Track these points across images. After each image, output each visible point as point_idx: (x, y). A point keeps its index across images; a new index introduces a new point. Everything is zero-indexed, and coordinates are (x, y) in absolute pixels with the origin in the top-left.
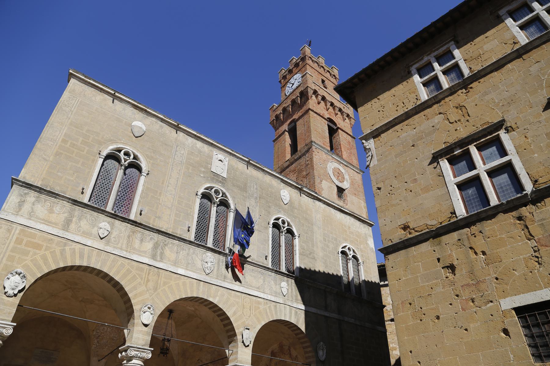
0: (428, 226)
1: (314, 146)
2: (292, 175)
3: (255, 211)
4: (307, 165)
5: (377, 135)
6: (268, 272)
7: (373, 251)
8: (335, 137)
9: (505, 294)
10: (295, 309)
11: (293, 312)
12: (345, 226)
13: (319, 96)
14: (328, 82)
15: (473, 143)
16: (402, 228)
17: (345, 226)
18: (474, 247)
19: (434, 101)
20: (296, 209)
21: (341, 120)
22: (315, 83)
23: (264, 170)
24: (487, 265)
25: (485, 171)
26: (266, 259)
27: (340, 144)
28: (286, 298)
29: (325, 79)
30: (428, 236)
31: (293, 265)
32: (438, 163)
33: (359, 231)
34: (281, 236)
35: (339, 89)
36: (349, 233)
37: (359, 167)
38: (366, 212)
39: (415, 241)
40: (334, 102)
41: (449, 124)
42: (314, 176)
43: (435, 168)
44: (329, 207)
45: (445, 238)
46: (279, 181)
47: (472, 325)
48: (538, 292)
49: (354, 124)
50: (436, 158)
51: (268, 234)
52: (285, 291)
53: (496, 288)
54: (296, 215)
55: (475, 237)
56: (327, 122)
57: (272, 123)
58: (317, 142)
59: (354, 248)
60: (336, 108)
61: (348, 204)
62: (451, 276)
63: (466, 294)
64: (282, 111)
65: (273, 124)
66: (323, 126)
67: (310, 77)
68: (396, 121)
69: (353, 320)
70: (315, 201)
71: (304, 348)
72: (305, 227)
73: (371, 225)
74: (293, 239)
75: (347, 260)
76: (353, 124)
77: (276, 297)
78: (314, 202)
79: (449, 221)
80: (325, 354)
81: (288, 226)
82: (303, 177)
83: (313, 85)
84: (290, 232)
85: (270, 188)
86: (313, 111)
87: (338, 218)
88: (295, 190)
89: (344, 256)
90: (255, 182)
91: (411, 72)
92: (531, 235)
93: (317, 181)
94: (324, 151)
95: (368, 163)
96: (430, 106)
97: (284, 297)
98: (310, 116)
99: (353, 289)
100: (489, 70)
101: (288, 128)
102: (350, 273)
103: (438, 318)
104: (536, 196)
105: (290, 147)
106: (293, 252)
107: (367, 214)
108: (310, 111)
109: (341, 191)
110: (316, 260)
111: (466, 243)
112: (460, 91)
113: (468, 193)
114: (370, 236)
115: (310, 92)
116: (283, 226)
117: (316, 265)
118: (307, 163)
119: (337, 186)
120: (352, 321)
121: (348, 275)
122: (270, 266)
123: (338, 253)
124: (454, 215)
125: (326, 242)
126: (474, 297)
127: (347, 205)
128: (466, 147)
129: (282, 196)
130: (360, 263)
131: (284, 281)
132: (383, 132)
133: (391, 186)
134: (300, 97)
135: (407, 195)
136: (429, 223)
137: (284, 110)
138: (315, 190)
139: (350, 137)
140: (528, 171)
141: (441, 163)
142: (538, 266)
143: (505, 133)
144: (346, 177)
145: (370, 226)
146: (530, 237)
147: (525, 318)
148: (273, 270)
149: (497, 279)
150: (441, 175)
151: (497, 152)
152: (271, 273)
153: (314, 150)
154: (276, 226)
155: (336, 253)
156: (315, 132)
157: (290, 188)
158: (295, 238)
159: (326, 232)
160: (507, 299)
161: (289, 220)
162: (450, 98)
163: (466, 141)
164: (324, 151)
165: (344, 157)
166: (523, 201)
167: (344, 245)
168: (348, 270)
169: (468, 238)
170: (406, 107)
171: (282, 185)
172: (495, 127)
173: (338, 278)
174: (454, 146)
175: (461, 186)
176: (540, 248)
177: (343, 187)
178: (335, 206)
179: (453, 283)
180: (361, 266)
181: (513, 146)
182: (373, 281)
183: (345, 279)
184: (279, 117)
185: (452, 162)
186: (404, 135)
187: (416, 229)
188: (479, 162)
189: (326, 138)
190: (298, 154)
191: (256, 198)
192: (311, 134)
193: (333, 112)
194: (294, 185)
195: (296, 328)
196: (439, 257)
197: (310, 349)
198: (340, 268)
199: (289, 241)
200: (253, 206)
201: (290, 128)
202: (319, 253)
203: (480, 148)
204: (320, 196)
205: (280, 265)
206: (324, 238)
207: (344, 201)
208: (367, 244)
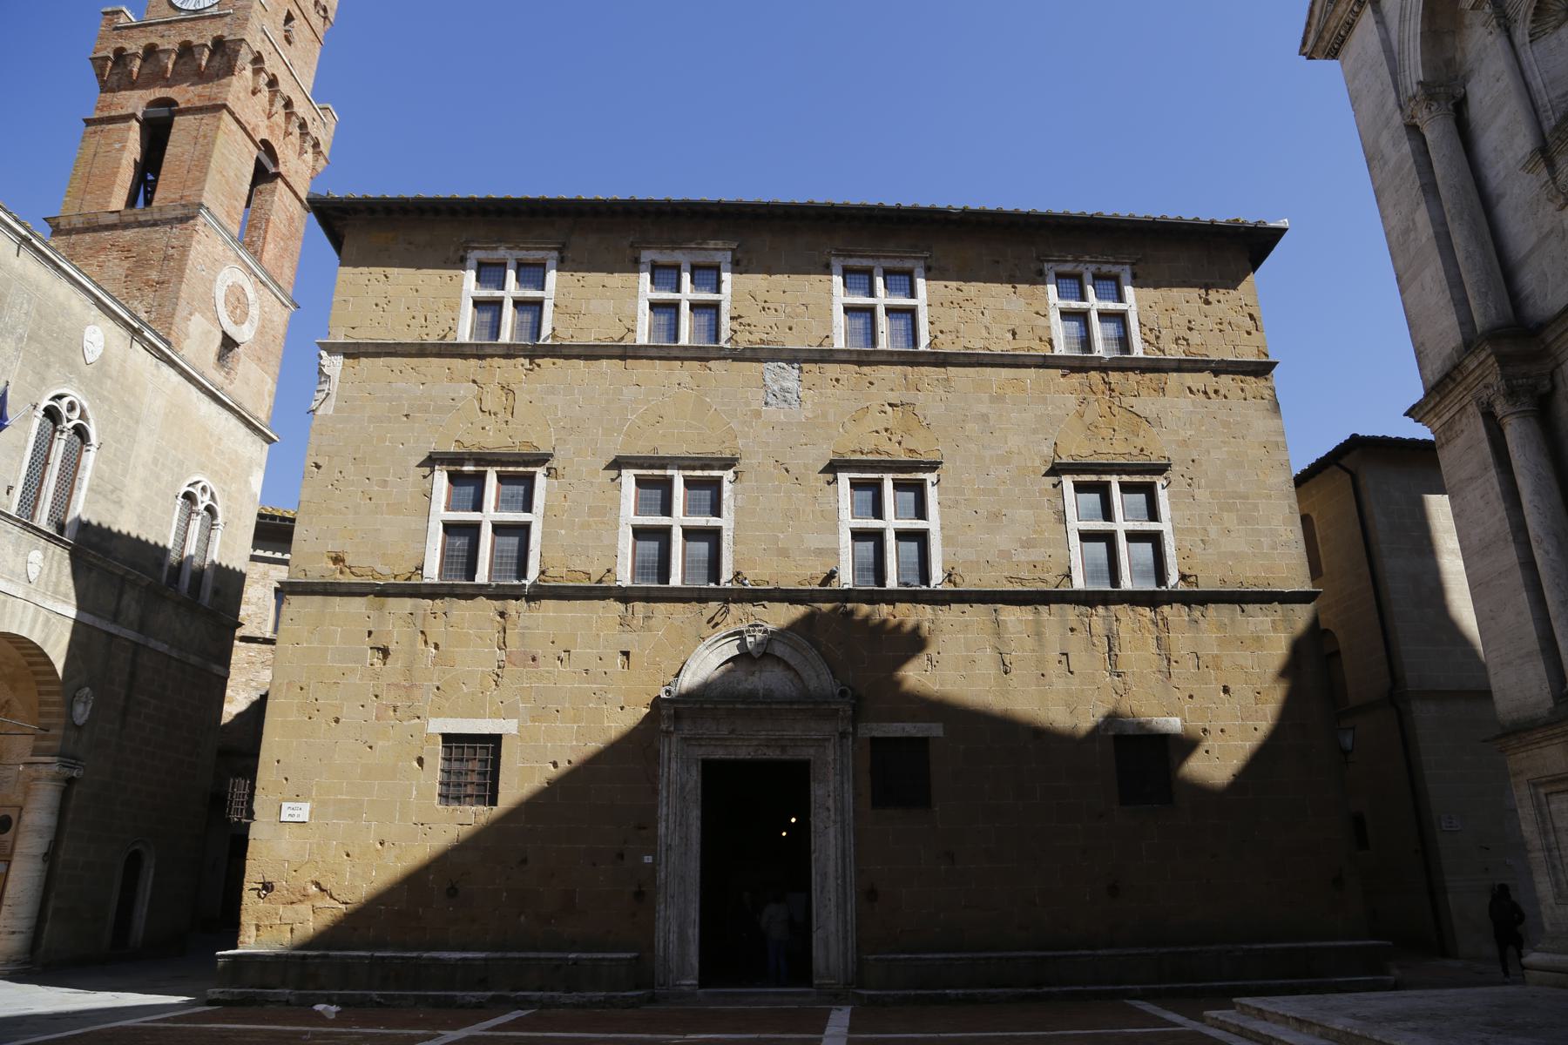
0: (374, 573)
1: (204, 217)
2: (114, 259)
3: (9, 371)
4: (167, 258)
5: (353, 354)
6: (5, 523)
7: (256, 499)
8: (261, 193)
9: (439, 712)
10: (46, 612)
11: (41, 619)
12: (211, 435)
13: (264, 74)
14: (301, 24)
15: (497, 466)
16: (332, 558)
18: (427, 633)
19: (475, 352)
20: (111, 378)
21: (295, 152)
22: (265, 34)
23: (58, 268)
24: (434, 665)
25: (491, 522)
26: (8, 493)
27: (268, 221)
28: (32, 586)
29: (296, 12)
30: (368, 589)
31: (66, 513)
32: (432, 472)
34: (56, 441)
35: (318, 205)
37: (290, 292)
38: (270, 406)
39: (344, 589)
40: (293, 101)
41: (479, 411)
42: (177, 299)
43: (425, 477)
44: (190, 385)
45: (393, 603)
46: (90, 302)
47: (380, 743)
48: (478, 721)
49: (323, 172)
50: (432, 461)
51: (27, 433)
52: (34, 572)
53: (432, 701)
54: (106, 393)
55: (435, 618)
56: (255, 152)
57: (99, 63)
58: (212, 210)
59: (214, 490)
60: (294, 118)
61: (236, 382)
62: (378, 664)
63: (388, 698)
64: (144, 52)
65: (102, 68)
66: (242, 163)
67: (260, 12)
68: (399, 349)
69: (167, 646)
70: (161, 363)
71: (40, 693)
72: (119, 425)
73: (270, 441)
74: (81, 449)
75: (190, 514)
76: (320, 170)
77: (10, 583)
78: (157, 365)
79: (409, 578)
80: (88, 713)
81: (80, 418)
82: (146, 283)
83: (258, 39)
84: (81, 432)
85: (63, 316)
86: (232, 114)
88: (121, 331)
89: (188, 503)
90: (28, 295)
91: (466, 259)
92: (504, 643)
93: (182, 310)
94: (221, 235)
95: (314, 405)
96: (465, 357)
97: (29, 585)
98: (218, 127)
99: (185, 579)
100: (575, 352)
101: (144, 113)
102: (188, 542)
103: (337, 721)
104: (534, 591)
105: (133, 170)
106: (73, 481)
107: (271, 411)
108: (225, 111)
109: (229, 344)
110: (122, 507)
111: (419, 623)
112: (522, 360)
113: (454, 544)
114: (260, 466)
115: (245, 58)
116: (67, 418)
117: (119, 518)
118: (171, 251)
119: (224, 333)
120: (164, 648)
121: (183, 548)
122: (13, 511)
123: (177, 497)
124: (420, 572)
125: (156, 466)
126: (399, 704)
127: (232, 382)
128: (483, 466)
129: (85, 342)
130: (218, 525)
131: (37, 549)
132: (367, 355)
133: (341, 472)
134: (210, 50)
135: (362, 502)
136: (379, 568)
137: (151, 51)
138: (169, 334)
139: (299, 204)
140: (543, 551)
141: (436, 473)
142: (494, 687)
143: (545, 475)
144: (254, 311)
145: (267, 442)
146: (502, 645)
147: (451, 748)
148: (18, 521)
149: (438, 688)
150: (428, 495)
151: (521, 498)
152: (12, 526)
153: (200, 228)
154: (52, 414)
155: (172, 495)
156: (218, 177)
157: (110, 323)
158: (89, 450)
159: (164, 443)
160: (439, 720)
161: (86, 405)
162: (503, 362)
163: (489, 458)
164: (221, 235)
165: (266, 256)
166: (517, 592)
167: (196, 479)
168: (186, 537)
169: (425, 615)
170: (426, 331)
171: (92, 313)
172: (536, 458)
173: (164, 551)
174: (467, 457)
175: (450, 528)
176: (507, 664)
177: (236, 339)
178: (203, 386)
179: (377, 676)
180: (219, 532)
181: (544, 502)
182: (231, 567)
183: (174, 557)
184: (128, 60)
185: (454, 478)
186: (402, 385)
187: (353, 570)
188: (489, 503)
189: (239, 199)
190: (152, 213)
191: (21, 339)
192: (205, 180)
193: (283, 125)
194: (122, 318)
195: (36, 652)
196: (372, 629)
197: (56, 698)
198: (170, 532)
199: (71, 453)
200: (9, 356)
201: (151, 116)
202: (134, 491)
203: (501, 478)
204: (176, 353)
205: (35, 508)
206: (155, 458)
207: (228, 373)
208: (247, 482)
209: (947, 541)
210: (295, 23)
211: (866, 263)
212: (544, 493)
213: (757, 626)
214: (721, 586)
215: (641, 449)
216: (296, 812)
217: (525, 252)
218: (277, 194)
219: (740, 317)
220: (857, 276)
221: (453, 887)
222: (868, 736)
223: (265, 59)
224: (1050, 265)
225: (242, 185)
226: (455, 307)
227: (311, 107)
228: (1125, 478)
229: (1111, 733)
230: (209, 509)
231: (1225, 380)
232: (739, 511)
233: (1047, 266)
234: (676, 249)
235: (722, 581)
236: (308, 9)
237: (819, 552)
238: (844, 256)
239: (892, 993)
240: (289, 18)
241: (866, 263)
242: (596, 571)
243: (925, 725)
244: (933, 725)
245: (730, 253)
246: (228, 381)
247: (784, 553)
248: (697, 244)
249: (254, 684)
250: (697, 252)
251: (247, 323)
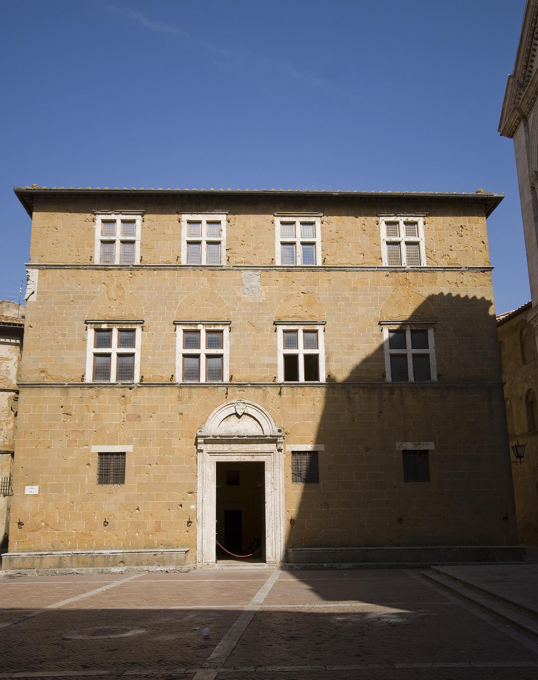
9: (96, 443)
47: (70, 457)
215: (185, 317)
216: (33, 490)
224: (383, 218)
226: (92, 245)
232: (232, 348)
237: (268, 365)
247: (252, 366)
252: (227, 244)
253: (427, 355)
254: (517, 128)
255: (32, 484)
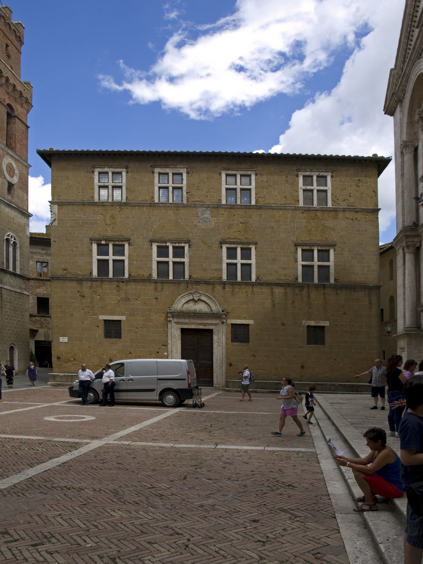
14: (12, 47)
17: (11, 218)
27: (15, 135)
33: (21, 221)
36: (13, 224)
47: (86, 322)
87: (7, 211)
91: (94, 172)
136: (79, 272)
144: (17, 172)
150: (91, 250)
160: (102, 316)
167: (8, 233)
185: (99, 245)
198: (4, 252)
207: (12, 196)
209: (257, 267)
210: (9, 48)
211: (234, 172)
212: (128, 251)
213: (196, 291)
214: (185, 280)
216: (64, 340)
217: (114, 169)
218: (16, 124)
219: (189, 192)
220: (231, 177)
221: (111, 359)
222: (231, 323)
223: (3, 71)
225: (4, 124)
227: (23, 85)
228: (320, 248)
229: (306, 325)
230: (14, 243)
231: (359, 216)
232: (190, 257)
233: (300, 173)
234: (167, 168)
235: (186, 278)
236: (13, 40)
237: (216, 270)
238: (226, 170)
239: (234, 389)
240: (7, 46)
241: (234, 172)
242: (146, 274)
243: (248, 321)
244: (250, 321)
245: (185, 169)
246: (12, 198)
247: (205, 270)
248: (174, 166)
249: (34, 293)
250: (174, 169)
251: (15, 176)
252: (187, 189)
253: (123, 261)
254: (395, 109)
255: (64, 336)
